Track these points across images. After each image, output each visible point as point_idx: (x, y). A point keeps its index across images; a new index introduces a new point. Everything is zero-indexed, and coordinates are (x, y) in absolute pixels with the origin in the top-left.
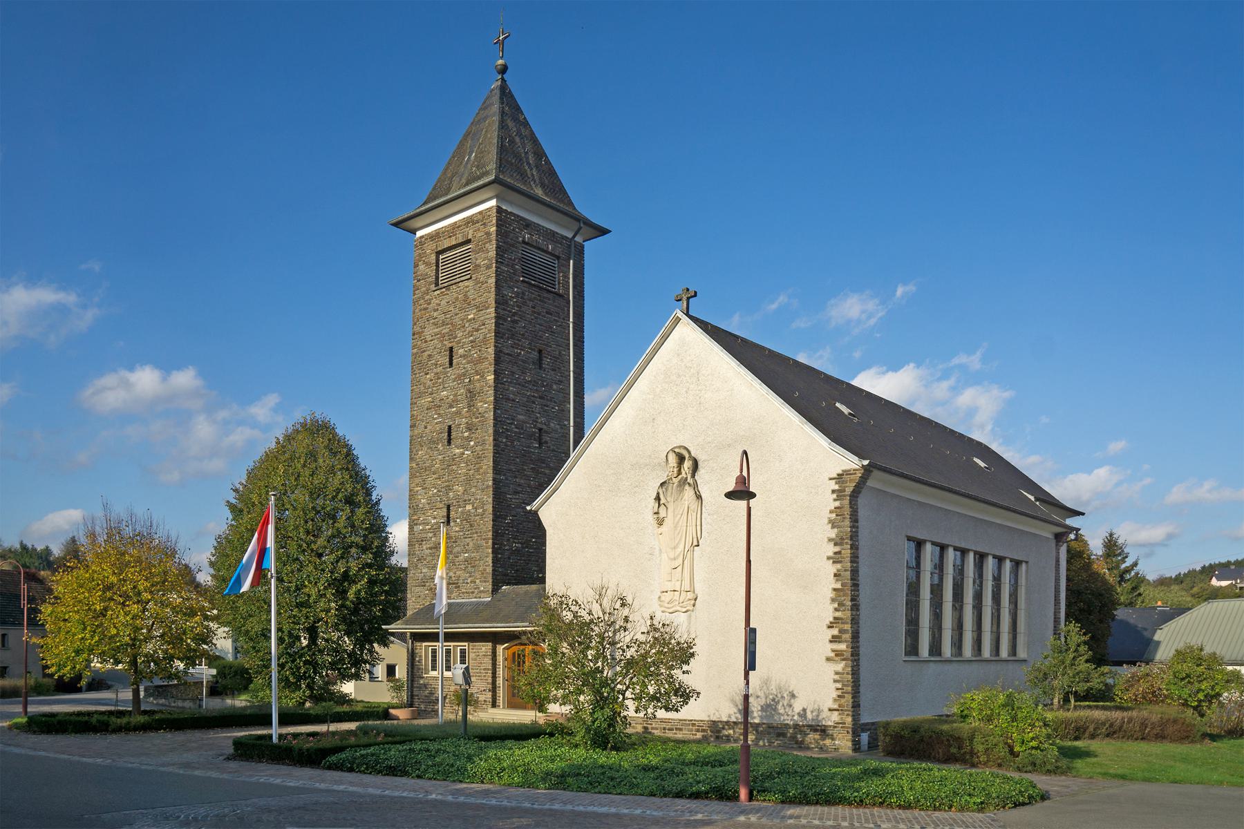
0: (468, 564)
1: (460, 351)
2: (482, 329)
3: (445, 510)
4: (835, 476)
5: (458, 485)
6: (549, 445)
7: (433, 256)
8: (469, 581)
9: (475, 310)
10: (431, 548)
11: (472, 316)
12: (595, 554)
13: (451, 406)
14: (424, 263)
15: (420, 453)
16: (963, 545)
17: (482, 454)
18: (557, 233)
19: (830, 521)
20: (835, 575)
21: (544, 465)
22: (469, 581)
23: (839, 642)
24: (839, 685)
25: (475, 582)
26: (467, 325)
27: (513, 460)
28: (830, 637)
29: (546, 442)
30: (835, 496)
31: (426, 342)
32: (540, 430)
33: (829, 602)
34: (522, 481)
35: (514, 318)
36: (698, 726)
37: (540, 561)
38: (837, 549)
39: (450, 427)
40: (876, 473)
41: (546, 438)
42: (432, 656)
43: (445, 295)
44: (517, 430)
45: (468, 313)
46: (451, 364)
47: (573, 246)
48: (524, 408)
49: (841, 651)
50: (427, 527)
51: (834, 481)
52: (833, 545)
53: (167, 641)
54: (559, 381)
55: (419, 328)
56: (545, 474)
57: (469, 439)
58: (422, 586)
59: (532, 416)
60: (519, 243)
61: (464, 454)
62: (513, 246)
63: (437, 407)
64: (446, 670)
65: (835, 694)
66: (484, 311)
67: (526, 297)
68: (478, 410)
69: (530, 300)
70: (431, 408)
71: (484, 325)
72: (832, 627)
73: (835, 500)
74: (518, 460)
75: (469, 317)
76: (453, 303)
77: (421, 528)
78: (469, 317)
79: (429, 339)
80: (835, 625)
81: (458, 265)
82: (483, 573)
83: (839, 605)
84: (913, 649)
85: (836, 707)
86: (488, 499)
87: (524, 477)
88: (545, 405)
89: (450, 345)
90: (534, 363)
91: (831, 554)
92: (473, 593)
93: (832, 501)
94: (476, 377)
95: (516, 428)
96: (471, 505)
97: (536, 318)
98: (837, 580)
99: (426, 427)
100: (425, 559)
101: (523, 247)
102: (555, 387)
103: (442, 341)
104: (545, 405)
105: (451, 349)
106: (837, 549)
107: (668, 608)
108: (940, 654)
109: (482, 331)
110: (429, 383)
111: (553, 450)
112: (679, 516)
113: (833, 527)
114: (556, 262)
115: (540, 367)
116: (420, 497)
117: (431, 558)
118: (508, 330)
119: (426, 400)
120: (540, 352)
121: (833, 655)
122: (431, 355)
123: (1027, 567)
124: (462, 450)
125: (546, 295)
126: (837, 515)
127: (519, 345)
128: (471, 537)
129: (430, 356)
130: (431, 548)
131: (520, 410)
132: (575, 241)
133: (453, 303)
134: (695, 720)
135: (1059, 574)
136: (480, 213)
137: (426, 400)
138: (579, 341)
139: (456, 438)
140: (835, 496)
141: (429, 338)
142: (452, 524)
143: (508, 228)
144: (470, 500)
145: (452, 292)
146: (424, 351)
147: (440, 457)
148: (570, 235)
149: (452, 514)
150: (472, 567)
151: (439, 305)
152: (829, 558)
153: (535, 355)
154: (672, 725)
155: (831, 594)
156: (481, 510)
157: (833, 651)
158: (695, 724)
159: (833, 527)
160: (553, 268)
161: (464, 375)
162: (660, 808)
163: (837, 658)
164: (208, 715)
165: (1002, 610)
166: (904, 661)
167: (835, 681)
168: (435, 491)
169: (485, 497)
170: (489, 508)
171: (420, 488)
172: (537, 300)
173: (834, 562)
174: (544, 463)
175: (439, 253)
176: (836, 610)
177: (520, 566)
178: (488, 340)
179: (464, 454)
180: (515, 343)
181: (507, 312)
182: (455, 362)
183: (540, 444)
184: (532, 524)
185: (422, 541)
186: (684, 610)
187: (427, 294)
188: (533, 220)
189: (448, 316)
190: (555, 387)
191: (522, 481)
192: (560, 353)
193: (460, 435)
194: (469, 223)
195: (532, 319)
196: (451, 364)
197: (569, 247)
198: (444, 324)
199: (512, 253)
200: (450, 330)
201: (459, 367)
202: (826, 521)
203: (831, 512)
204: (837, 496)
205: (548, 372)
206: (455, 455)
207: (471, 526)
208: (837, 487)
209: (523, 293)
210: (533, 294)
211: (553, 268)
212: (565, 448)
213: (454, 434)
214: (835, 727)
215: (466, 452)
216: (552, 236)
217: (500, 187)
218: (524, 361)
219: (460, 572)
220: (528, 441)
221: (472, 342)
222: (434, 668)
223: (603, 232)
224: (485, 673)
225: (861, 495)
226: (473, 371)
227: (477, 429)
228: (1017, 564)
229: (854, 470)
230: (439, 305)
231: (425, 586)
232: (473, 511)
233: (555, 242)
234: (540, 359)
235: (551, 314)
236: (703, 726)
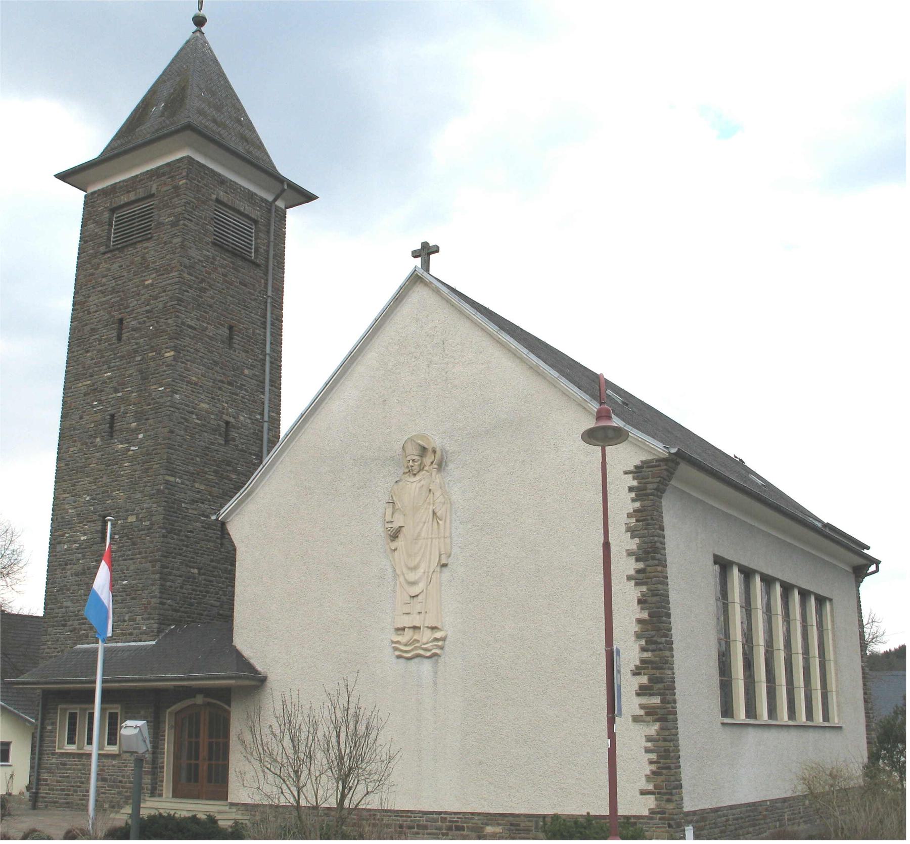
1: (133, 323)
2: (162, 297)
4: (632, 468)
5: (119, 490)
6: (237, 443)
7: (106, 215)
8: (127, 618)
9: (154, 275)
10: (77, 575)
11: (150, 281)
12: (303, 578)
13: (116, 391)
14: (95, 222)
15: (72, 449)
16: (769, 572)
18: (257, 195)
19: (629, 529)
20: (640, 602)
21: (228, 468)
22: (127, 618)
23: (651, 695)
24: (653, 756)
25: (134, 620)
26: (142, 292)
27: (192, 459)
28: (636, 687)
29: (234, 440)
30: (633, 495)
31: (89, 313)
32: (227, 423)
33: (633, 638)
34: (202, 487)
35: (201, 285)
36: (450, 821)
37: (221, 593)
38: (641, 565)
39: (112, 416)
40: (684, 469)
41: (234, 434)
43: (118, 258)
44: (199, 422)
45: (145, 278)
46: (119, 338)
47: (273, 210)
48: (208, 395)
49: (654, 708)
51: (631, 476)
52: (634, 560)
54: (251, 365)
55: (81, 297)
56: (231, 480)
57: (136, 431)
59: (218, 405)
60: (211, 200)
61: (129, 450)
62: (203, 202)
63: (98, 392)
65: (648, 769)
66: (166, 276)
67: (216, 263)
68: (150, 394)
69: (222, 267)
70: (89, 394)
71: (164, 291)
72: (639, 674)
73: (633, 500)
74: (198, 459)
75: (147, 283)
76: (128, 266)
77: (66, 547)
78: (147, 283)
79: (94, 310)
80: (643, 671)
81: (137, 224)
82: (146, 608)
83: (646, 642)
84: (727, 710)
85: (650, 787)
87: (205, 482)
88: (233, 394)
89: (120, 316)
90: (223, 342)
91: (632, 572)
92: (131, 634)
93: (630, 501)
94: (150, 355)
95: (198, 419)
96: (135, 516)
97: (228, 288)
98: (642, 609)
99: (81, 418)
100: (68, 590)
101: (216, 206)
102: (246, 372)
103: (109, 313)
104: (233, 394)
105: (121, 321)
106: (641, 565)
107: (406, 652)
108: (732, 717)
109: (162, 299)
110: (89, 362)
111: (242, 450)
112: (421, 525)
113: (632, 537)
114: (254, 227)
115: (231, 346)
116: (67, 507)
117: (76, 587)
118: (193, 299)
119: (85, 383)
120: (231, 328)
121: (642, 712)
122: (94, 329)
123: (832, 605)
124: (127, 445)
125: (240, 263)
126: (637, 521)
127: (206, 318)
128: (132, 559)
129: (92, 329)
130: (77, 575)
131: (202, 397)
132: (276, 206)
133: (128, 266)
134: (445, 813)
135: (862, 617)
136: (168, 164)
137: (85, 383)
138: (277, 319)
139: (121, 431)
140: (633, 495)
141: (93, 308)
143: (199, 182)
144: (134, 510)
145: (126, 255)
146: (86, 325)
147: (98, 455)
148: (270, 198)
151: (109, 269)
152: (629, 578)
153: (225, 331)
154: (411, 821)
155: (635, 628)
157: (642, 707)
158: (446, 818)
159: (632, 537)
160: (249, 233)
161: (135, 351)
163: (648, 718)
165: (811, 660)
166: (723, 724)
167: (648, 751)
168: (88, 498)
169: (155, 505)
171: (68, 495)
172: (230, 267)
173: (637, 584)
174: (229, 466)
175: (113, 211)
176: (643, 649)
177: (194, 599)
178: (169, 310)
179: (129, 450)
180: (201, 316)
181: (193, 278)
182: (125, 337)
183: (227, 442)
184: (212, 544)
185: (66, 565)
186: (428, 654)
187: (95, 257)
188: (229, 177)
189: (119, 282)
190: (246, 372)
191: (202, 487)
192: (254, 332)
193: (126, 426)
194: (151, 177)
195: (223, 289)
196: (119, 338)
197: (269, 211)
198: (114, 291)
199: (203, 211)
200: (121, 299)
201: (130, 343)
202: (623, 528)
203: (629, 516)
204: (636, 495)
205: (239, 353)
206: (117, 452)
207: (134, 544)
208: (635, 483)
209: (214, 258)
210: (225, 260)
211: (249, 233)
212: (257, 449)
213: (117, 425)
214: (651, 818)
215: (132, 448)
216: (251, 196)
218: (211, 338)
220: (212, 437)
221: (147, 312)
223: (308, 197)
225: (664, 495)
226: (146, 347)
227: (147, 419)
228: (821, 601)
229: (657, 461)
230: (109, 269)
233: (253, 204)
234: (231, 338)
235: (245, 286)
236: (457, 822)
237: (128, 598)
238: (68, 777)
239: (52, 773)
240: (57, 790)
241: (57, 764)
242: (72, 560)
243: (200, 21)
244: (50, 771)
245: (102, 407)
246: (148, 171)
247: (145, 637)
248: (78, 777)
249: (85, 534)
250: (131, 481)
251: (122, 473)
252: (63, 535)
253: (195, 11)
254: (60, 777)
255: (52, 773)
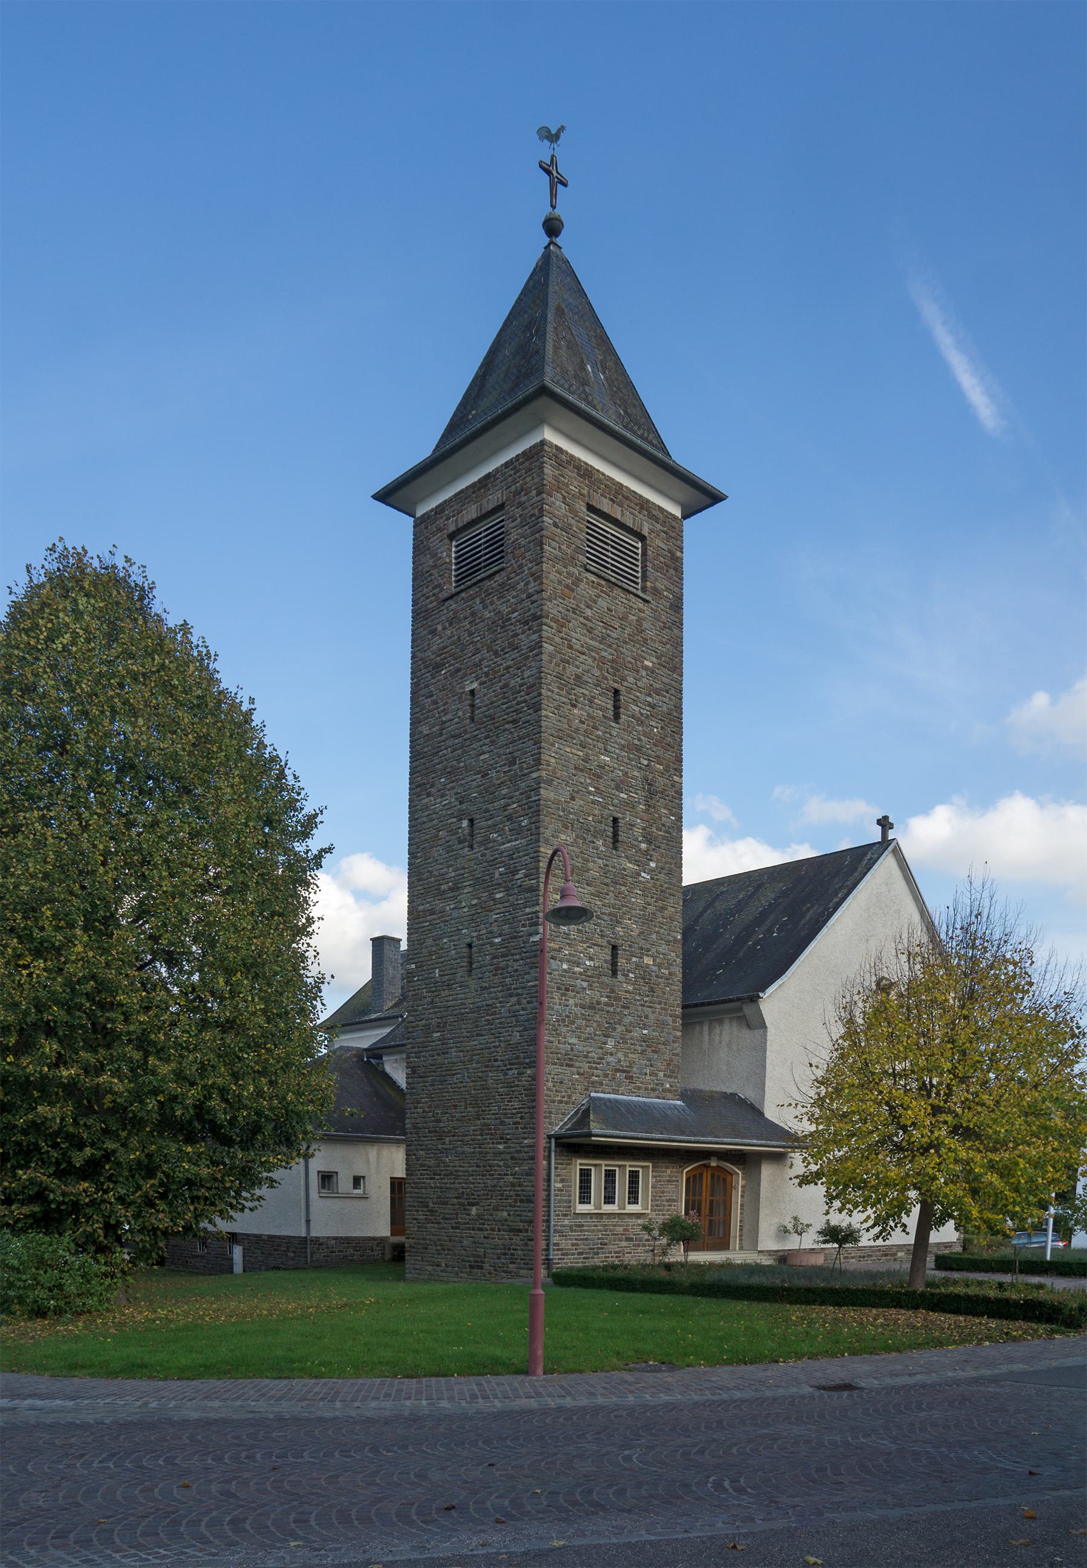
0: (647, 1046)
2: (665, 697)
3: (608, 951)
17: (668, 888)
25: (656, 1075)
42: (614, 1182)
50: (577, 969)
53: (902, 1058)
58: (567, 1065)
64: (605, 1203)
77: (565, 966)
82: (668, 1065)
86: (676, 958)
128: (471, 643)
142: (620, 977)
148: (676, 511)
149: (621, 961)
150: (653, 1051)
156: (667, 972)
162: (264, 1395)
164: (1034, 1259)
170: (678, 971)
185: (567, 990)
206: (625, 870)
207: (652, 990)
217: (692, 489)
219: (634, 1056)
222: (585, 1198)
224: (669, 1206)
231: (571, 1066)
232: (655, 968)
237: (650, 1050)
238: (587, 1239)
239: (566, 1236)
240: (573, 1254)
241: (571, 1227)
242: (575, 986)
243: (552, 227)
244: (562, 1234)
245: (601, 800)
246: (641, 496)
247: (669, 1095)
248: (598, 1239)
249: (591, 959)
250: (644, 915)
251: (633, 900)
252: (559, 950)
253: (546, 211)
254: (576, 1239)
255: (566, 1236)
